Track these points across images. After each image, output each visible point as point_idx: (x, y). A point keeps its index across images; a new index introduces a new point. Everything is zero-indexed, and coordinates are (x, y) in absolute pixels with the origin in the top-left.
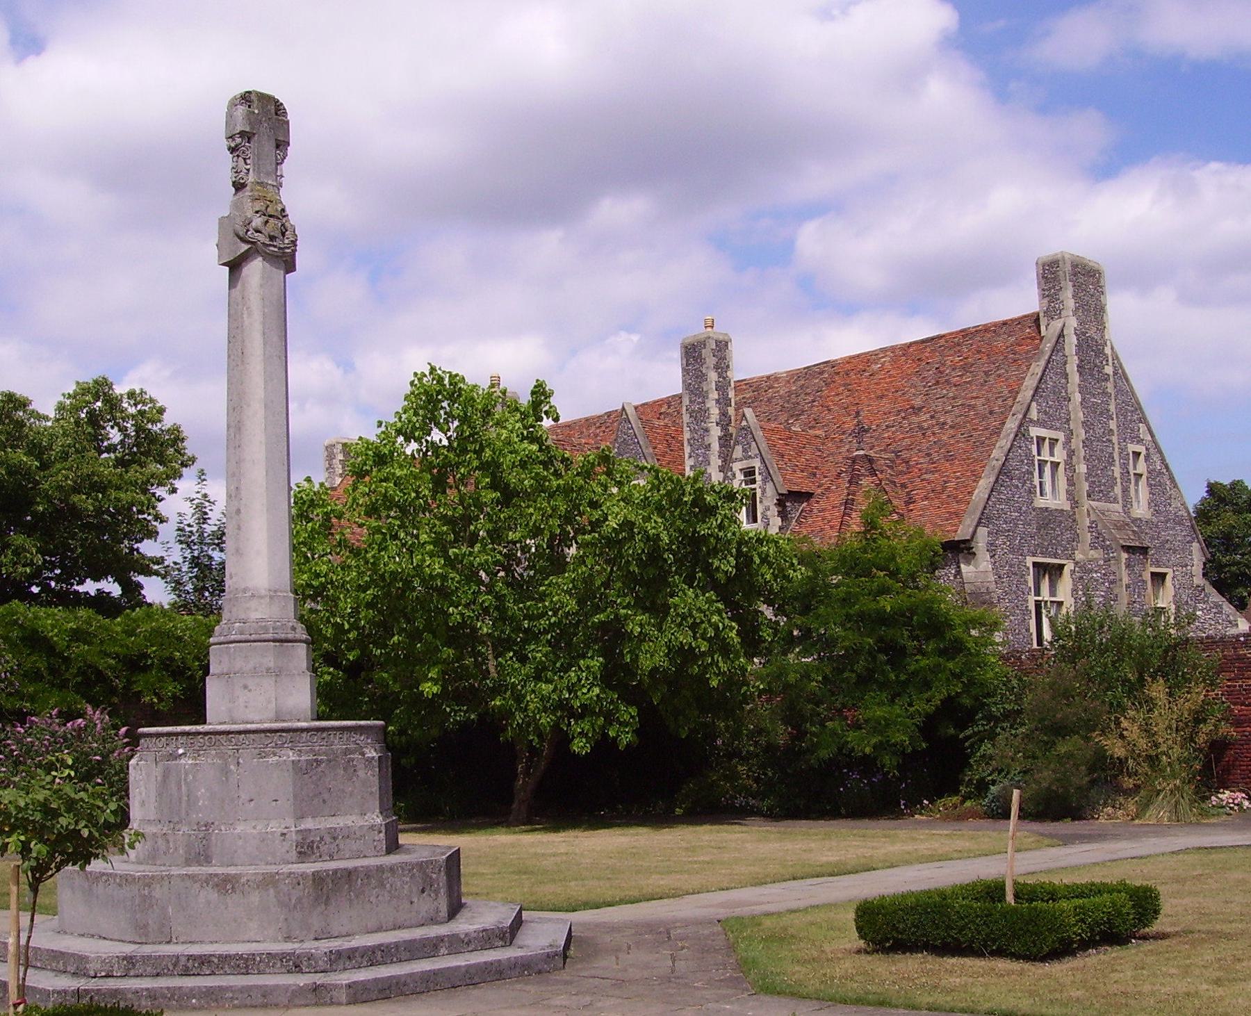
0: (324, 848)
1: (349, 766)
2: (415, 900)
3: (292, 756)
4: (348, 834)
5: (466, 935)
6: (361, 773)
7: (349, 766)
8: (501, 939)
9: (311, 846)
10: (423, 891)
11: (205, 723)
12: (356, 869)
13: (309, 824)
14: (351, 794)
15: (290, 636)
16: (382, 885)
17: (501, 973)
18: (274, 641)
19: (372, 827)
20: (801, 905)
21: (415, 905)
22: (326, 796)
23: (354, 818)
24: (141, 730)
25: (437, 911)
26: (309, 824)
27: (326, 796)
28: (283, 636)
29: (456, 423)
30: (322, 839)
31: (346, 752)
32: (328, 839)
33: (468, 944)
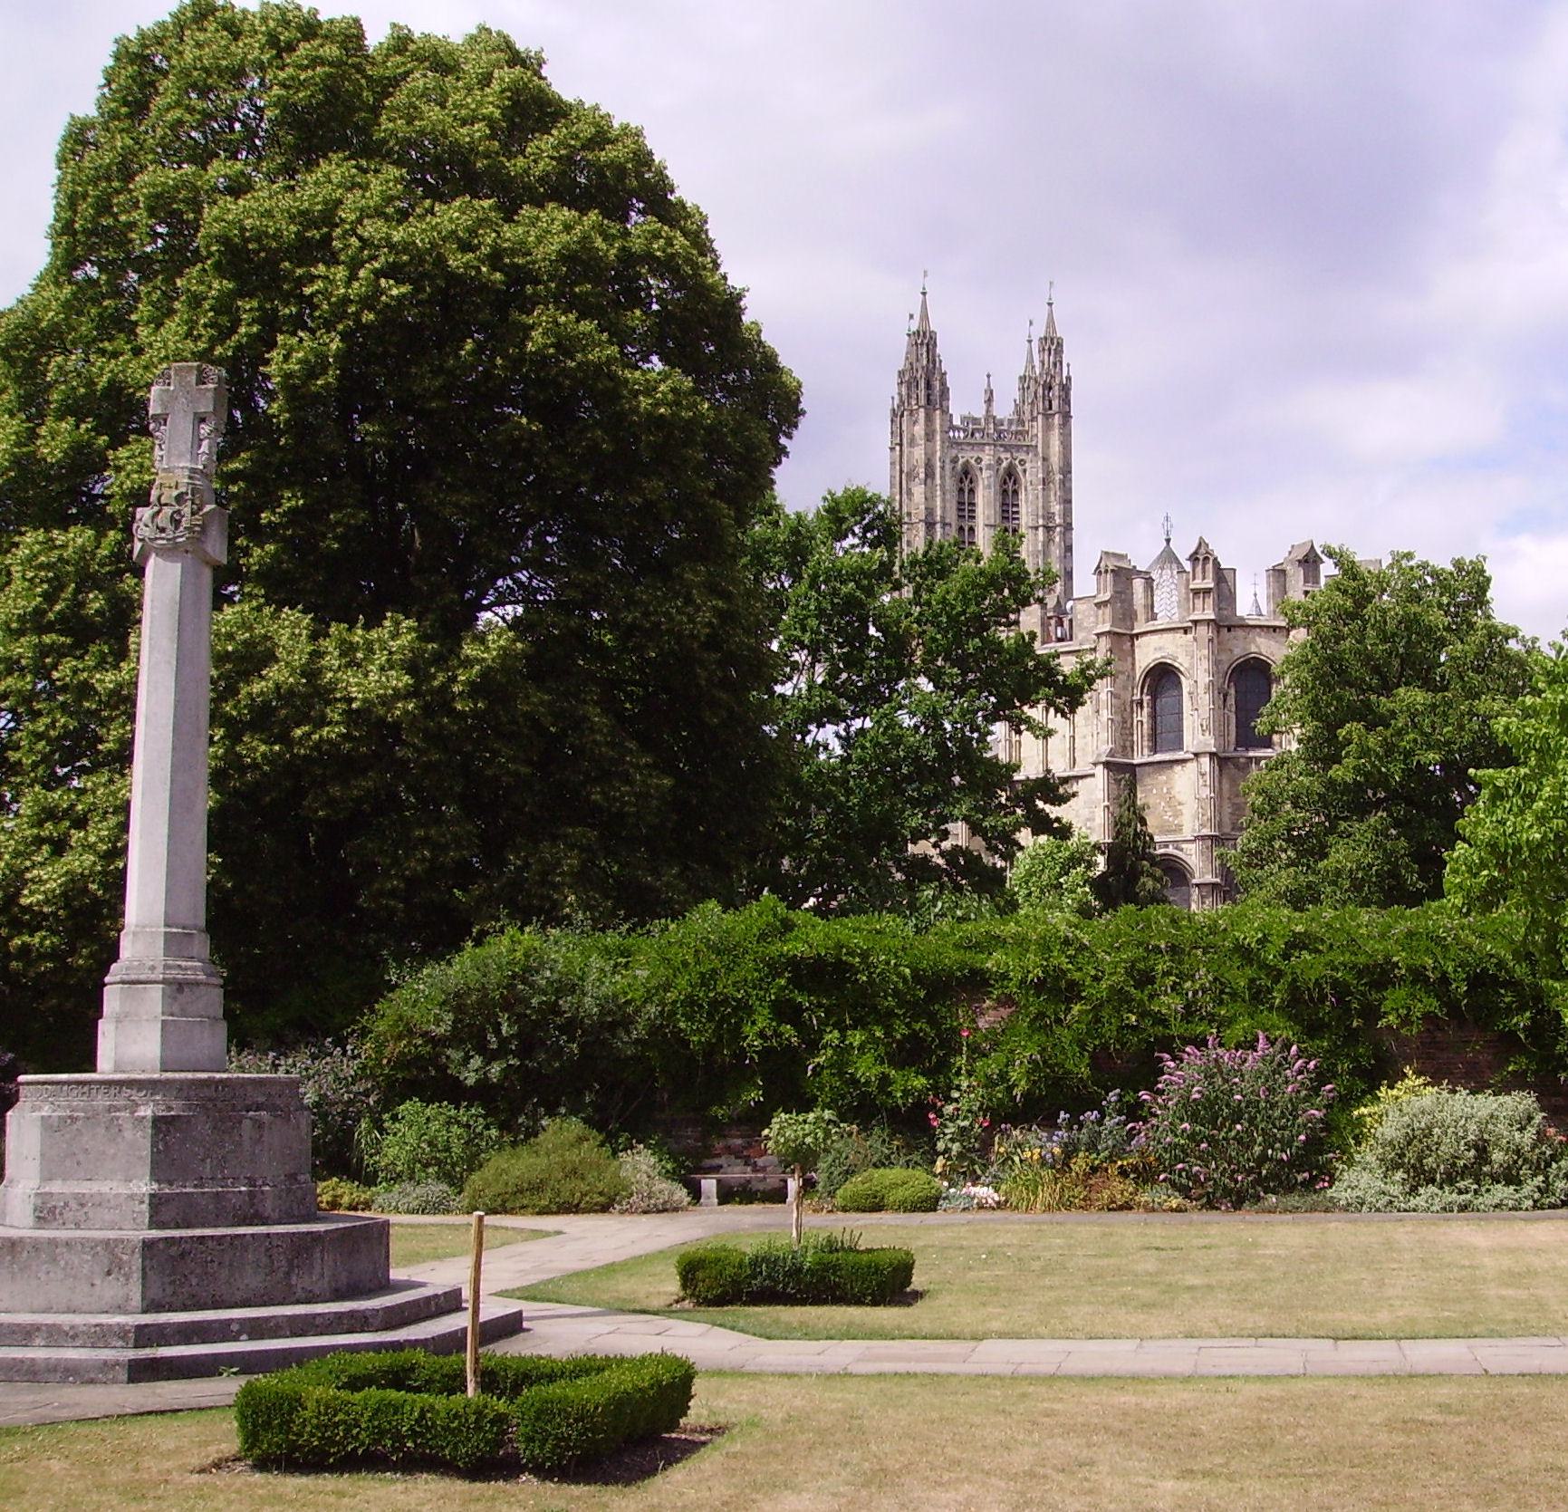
0: (68, 1215)
1: (114, 1127)
2: (98, 1282)
3: (46, 1111)
4: (100, 1202)
5: (72, 1327)
6: (128, 1134)
7: (114, 1127)
8: (122, 1338)
9: (52, 1210)
10: (109, 1273)
11: (94, 1070)
12: (21, 1240)
13: (56, 1187)
14: (114, 1157)
15: (143, 977)
16: (54, 1260)
17: (35, 1374)
18: (123, 982)
19: (131, 1197)
20: (1277, 1370)
21: (97, 1289)
22: (81, 1157)
23: (114, 1184)
24: (22, 1078)
25: (127, 1299)
26: (56, 1187)
27: (81, 1157)
28: (133, 977)
29: (56, 675)
30: (66, 1204)
31: (110, 1109)
32: (73, 1204)
33: (74, 1337)
